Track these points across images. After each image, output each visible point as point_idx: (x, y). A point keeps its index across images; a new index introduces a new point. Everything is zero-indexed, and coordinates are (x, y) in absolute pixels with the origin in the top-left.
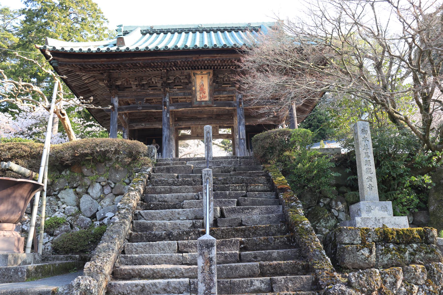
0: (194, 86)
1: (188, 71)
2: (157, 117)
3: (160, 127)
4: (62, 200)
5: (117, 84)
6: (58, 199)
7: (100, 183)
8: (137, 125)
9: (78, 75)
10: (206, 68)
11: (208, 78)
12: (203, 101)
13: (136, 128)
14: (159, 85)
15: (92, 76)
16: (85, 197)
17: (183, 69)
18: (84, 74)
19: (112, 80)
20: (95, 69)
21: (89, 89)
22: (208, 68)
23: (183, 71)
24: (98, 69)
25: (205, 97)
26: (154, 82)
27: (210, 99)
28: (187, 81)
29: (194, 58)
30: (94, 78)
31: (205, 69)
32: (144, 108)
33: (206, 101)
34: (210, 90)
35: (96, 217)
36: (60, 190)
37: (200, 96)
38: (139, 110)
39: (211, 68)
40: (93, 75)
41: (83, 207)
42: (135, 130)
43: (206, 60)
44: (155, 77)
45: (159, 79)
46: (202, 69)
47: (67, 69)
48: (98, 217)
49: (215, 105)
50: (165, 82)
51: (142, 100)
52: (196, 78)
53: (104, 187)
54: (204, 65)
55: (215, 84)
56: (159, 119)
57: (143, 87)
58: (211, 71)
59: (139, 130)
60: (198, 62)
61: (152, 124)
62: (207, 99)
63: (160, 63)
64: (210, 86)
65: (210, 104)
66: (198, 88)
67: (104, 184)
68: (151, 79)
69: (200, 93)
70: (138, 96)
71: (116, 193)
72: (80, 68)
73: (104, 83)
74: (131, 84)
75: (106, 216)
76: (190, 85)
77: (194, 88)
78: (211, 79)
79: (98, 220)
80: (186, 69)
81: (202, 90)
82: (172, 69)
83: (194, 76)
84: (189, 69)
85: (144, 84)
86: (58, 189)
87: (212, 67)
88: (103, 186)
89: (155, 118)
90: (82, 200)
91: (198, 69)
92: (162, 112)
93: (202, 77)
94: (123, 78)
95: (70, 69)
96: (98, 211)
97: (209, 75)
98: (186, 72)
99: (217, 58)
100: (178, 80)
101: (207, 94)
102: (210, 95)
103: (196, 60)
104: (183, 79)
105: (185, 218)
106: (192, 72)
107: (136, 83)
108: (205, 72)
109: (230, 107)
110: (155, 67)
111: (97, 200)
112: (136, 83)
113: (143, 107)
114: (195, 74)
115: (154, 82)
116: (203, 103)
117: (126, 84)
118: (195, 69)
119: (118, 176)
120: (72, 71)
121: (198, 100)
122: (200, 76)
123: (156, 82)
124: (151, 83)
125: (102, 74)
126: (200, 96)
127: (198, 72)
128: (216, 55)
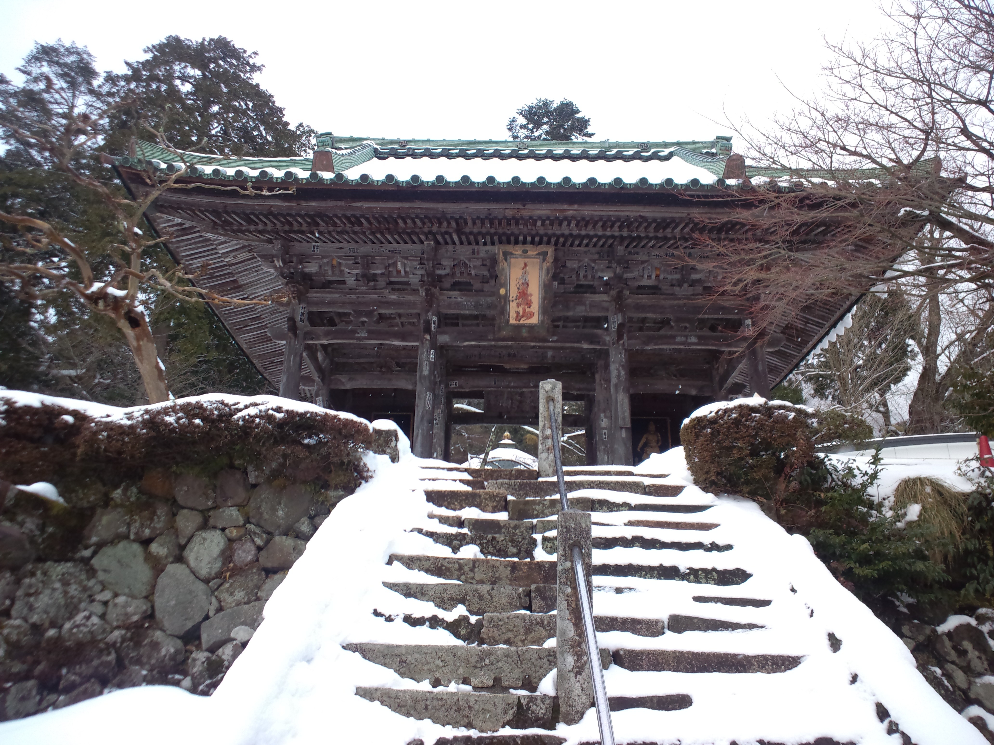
0: (504, 285)
1: (489, 247)
2: (404, 360)
3: (410, 387)
4: (101, 576)
5: (307, 270)
6: (92, 572)
7: (223, 530)
8: (350, 379)
9: (209, 240)
10: (537, 240)
11: (541, 268)
12: (523, 326)
13: (348, 386)
14: (414, 280)
15: (244, 247)
16: (173, 569)
17: (477, 243)
18: (222, 239)
19: (295, 259)
20: (252, 228)
21: (235, 281)
22: (540, 243)
23: (476, 247)
24: (261, 227)
25: (531, 315)
26: (402, 272)
27: (543, 322)
28: (486, 273)
29: (508, 210)
30: (250, 251)
31: (532, 242)
32: (372, 334)
33: (531, 327)
34: (544, 299)
35: (199, 638)
36: (100, 546)
37: (518, 313)
38: (359, 339)
39: (548, 243)
40: (246, 243)
41: (164, 601)
42: (346, 391)
43: (540, 218)
44: (406, 258)
45: (415, 263)
46: (524, 242)
47: (180, 221)
48: (204, 637)
49: (555, 338)
50: (430, 274)
51: (369, 314)
52: (509, 266)
53: (236, 545)
54: (533, 232)
55: (555, 284)
56: (410, 367)
57: (372, 283)
58: (550, 250)
59: (354, 391)
60: (517, 224)
61: (390, 380)
62: (534, 320)
63: (421, 220)
64: (546, 287)
65: (543, 333)
66: (514, 292)
67: (234, 533)
68: (395, 264)
69: (518, 305)
70: (360, 303)
71: (269, 565)
72: (215, 222)
73: (275, 267)
74: (342, 271)
75: (232, 635)
76: (492, 282)
77: (502, 291)
78: (548, 270)
79: (204, 645)
80: (485, 244)
81: (523, 295)
82: (449, 240)
83: (506, 260)
84: (493, 244)
85: (375, 275)
86: (94, 539)
87: (553, 240)
88: (231, 541)
89: (398, 365)
90: (163, 580)
91: (516, 242)
92: (416, 348)
93: (526, 265)
94: (323, 257)
95: (188, 224)
96: (207, 617)
97: (544, 260)
98: (484, 251)
99: (570, 213)
100: (463, 269)
101: (535, 307)
102: (544, 310)
103: (514, 218)
104: (475, 267)
105: (491, 683)
106: (498, 250)
107: (356, 271)
108: (532, 251)
109: (591, 343)
110: (408, 236)
111: (206, 581)
112: (356, 271)
113: (369, 332)
114: (506, 255)
115: (402, 272)
116: (524, 330)
117: (330, 272)
118: (509, 242)
119: (280, 513)
120: (192, 227)
121: (512, 321)
122: (521, 262)
123: (406, 272)
124: (395, 273)
125: (270, 241)
126: (518, 313)
127: (518, 250)
128: (565, 207)
